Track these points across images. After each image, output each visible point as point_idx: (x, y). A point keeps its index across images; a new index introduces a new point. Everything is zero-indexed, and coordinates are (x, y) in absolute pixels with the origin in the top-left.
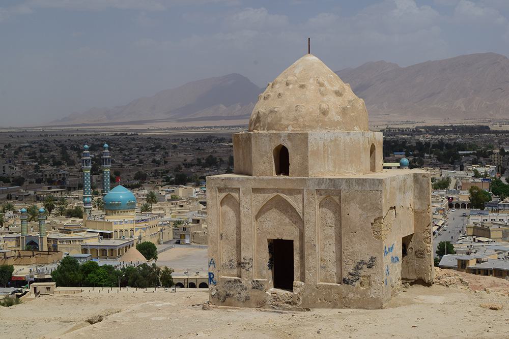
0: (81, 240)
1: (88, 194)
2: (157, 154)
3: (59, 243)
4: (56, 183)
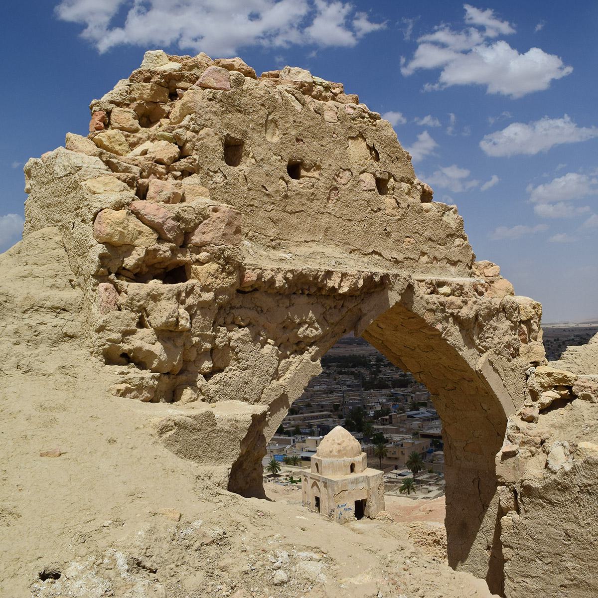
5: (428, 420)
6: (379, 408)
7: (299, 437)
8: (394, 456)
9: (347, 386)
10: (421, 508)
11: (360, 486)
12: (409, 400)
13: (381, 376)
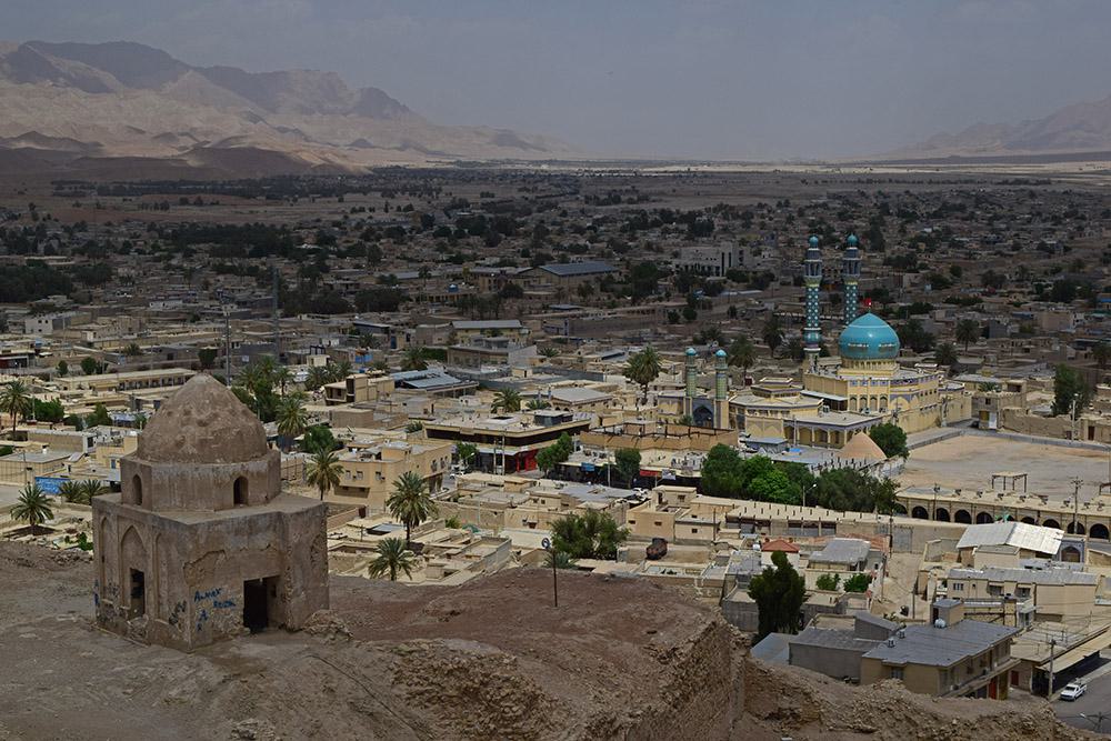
0: (785, 411)
1: (813, 326)
2: (1059, 230)
3: (747, 413)
4: (830, 287)
5: (449, 394)
6: (320, 361)
7: (105, 430)
8: (358, 484)
9: (239, 303)
10: (430, 606)
11: (262, 541)
12: (401, 342)
13: (329, 280)
